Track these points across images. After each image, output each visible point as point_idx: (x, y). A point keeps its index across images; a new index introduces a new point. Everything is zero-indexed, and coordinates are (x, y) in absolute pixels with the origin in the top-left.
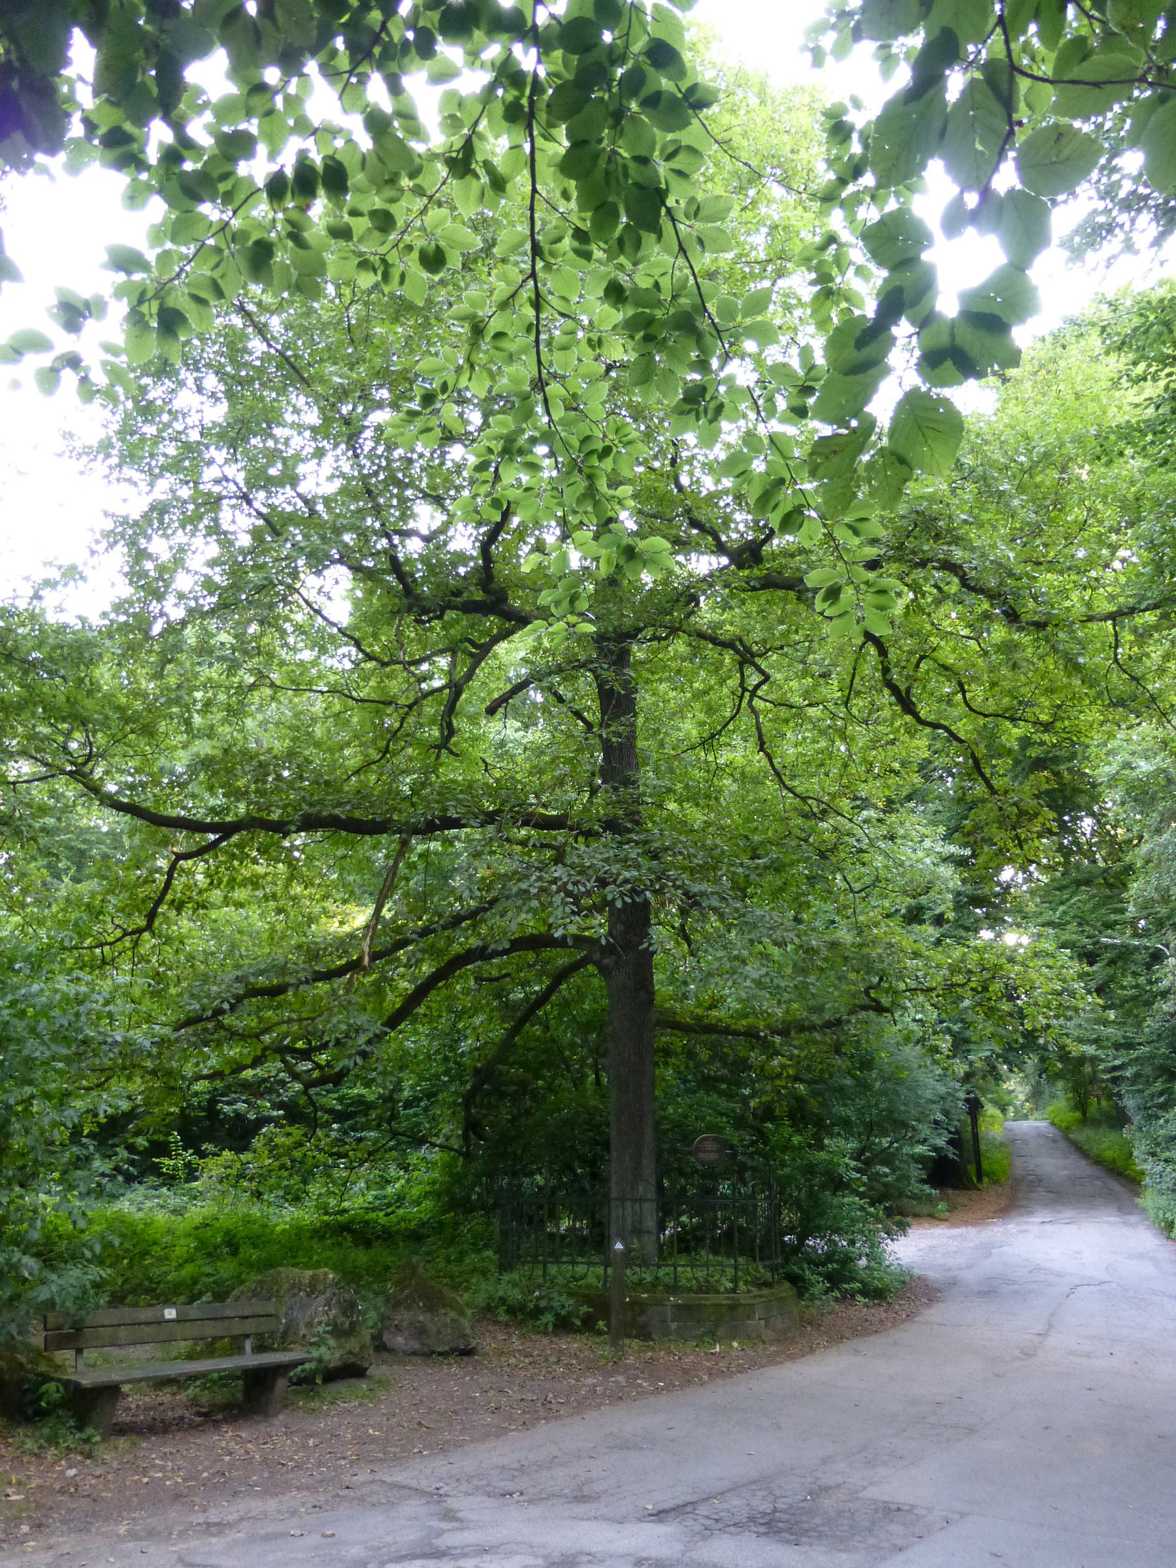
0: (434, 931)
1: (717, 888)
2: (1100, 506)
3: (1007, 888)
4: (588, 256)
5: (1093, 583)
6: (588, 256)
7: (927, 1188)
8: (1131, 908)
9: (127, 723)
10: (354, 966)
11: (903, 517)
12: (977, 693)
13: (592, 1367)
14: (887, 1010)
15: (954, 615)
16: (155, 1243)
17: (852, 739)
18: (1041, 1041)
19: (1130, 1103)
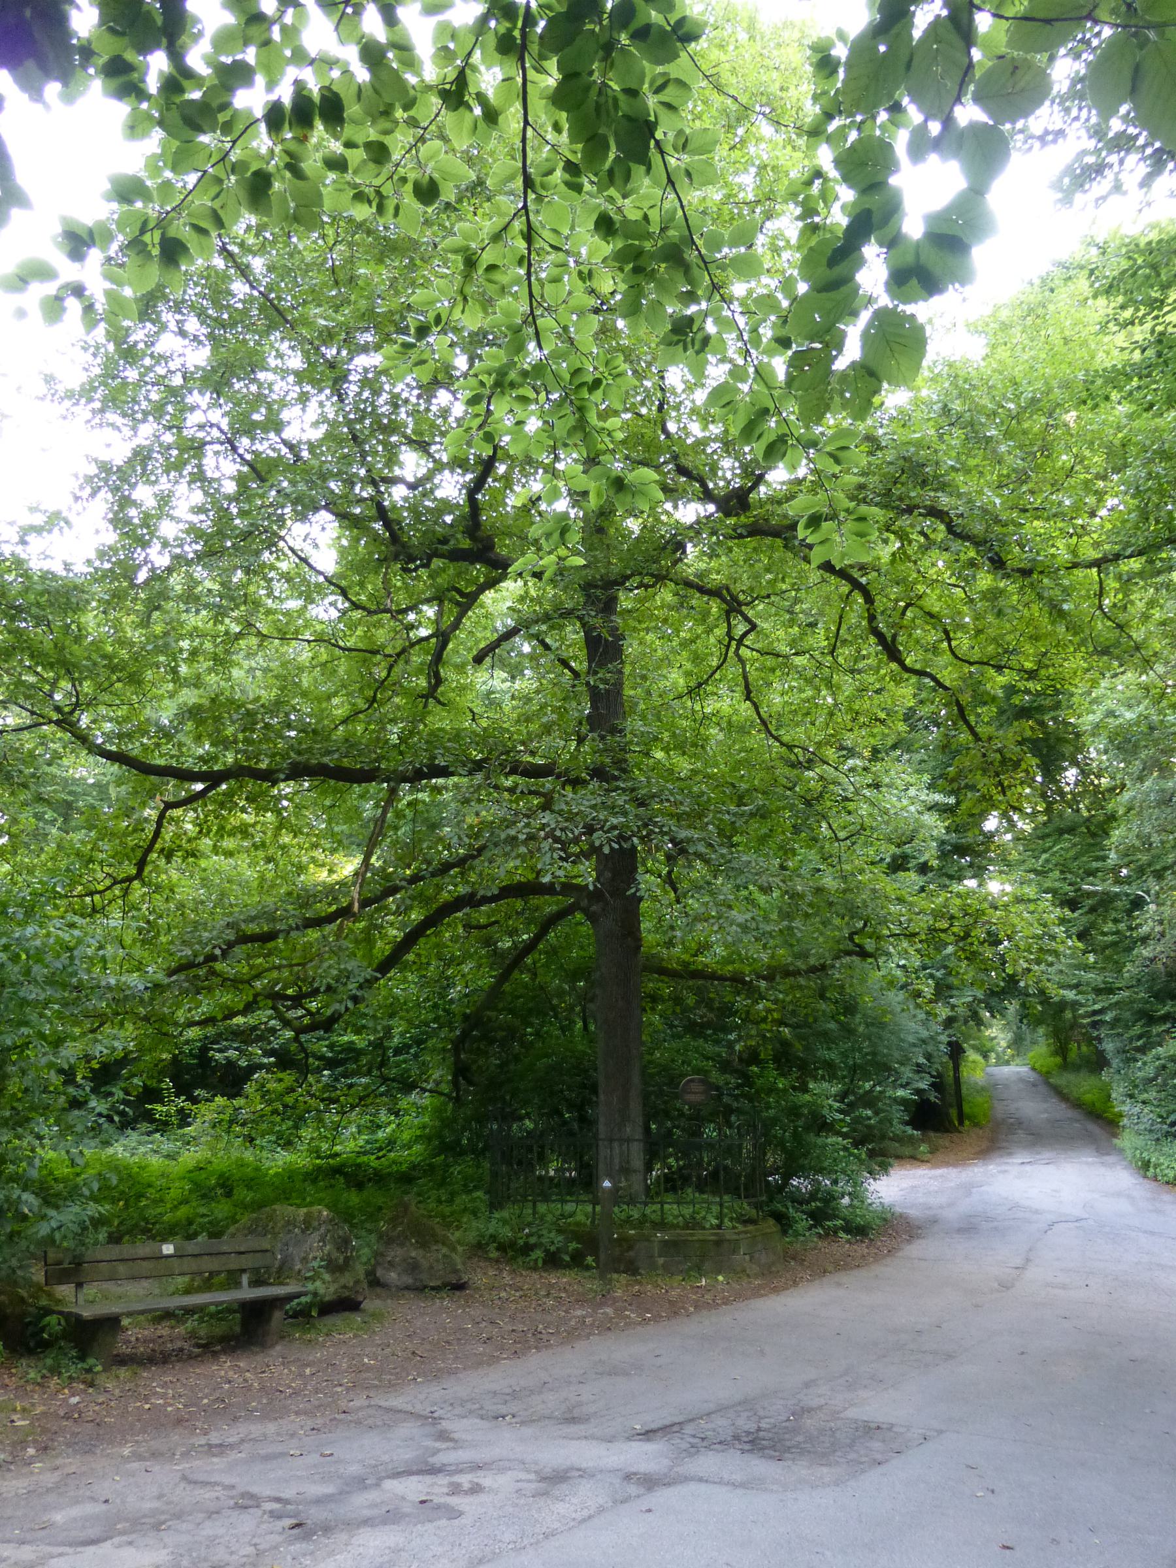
0: (422, 878)
1: (704, 834)
2: (1087, 453)
3: (990, 836)
4: (578, 188)
5: (1079, 531)
6: (578, 188)
7: (909, 1130)
8: (1113, 855)
9: (113, 672)
10: (345, 912)
11: (890, 463)
12: (963, 642)
13: (581, 1301)
14: (870, 955)
15: (940, 563)
16: (150, 1186)
17: (839, 688)
18: (1022, 984)
19: (1109, 1046)
